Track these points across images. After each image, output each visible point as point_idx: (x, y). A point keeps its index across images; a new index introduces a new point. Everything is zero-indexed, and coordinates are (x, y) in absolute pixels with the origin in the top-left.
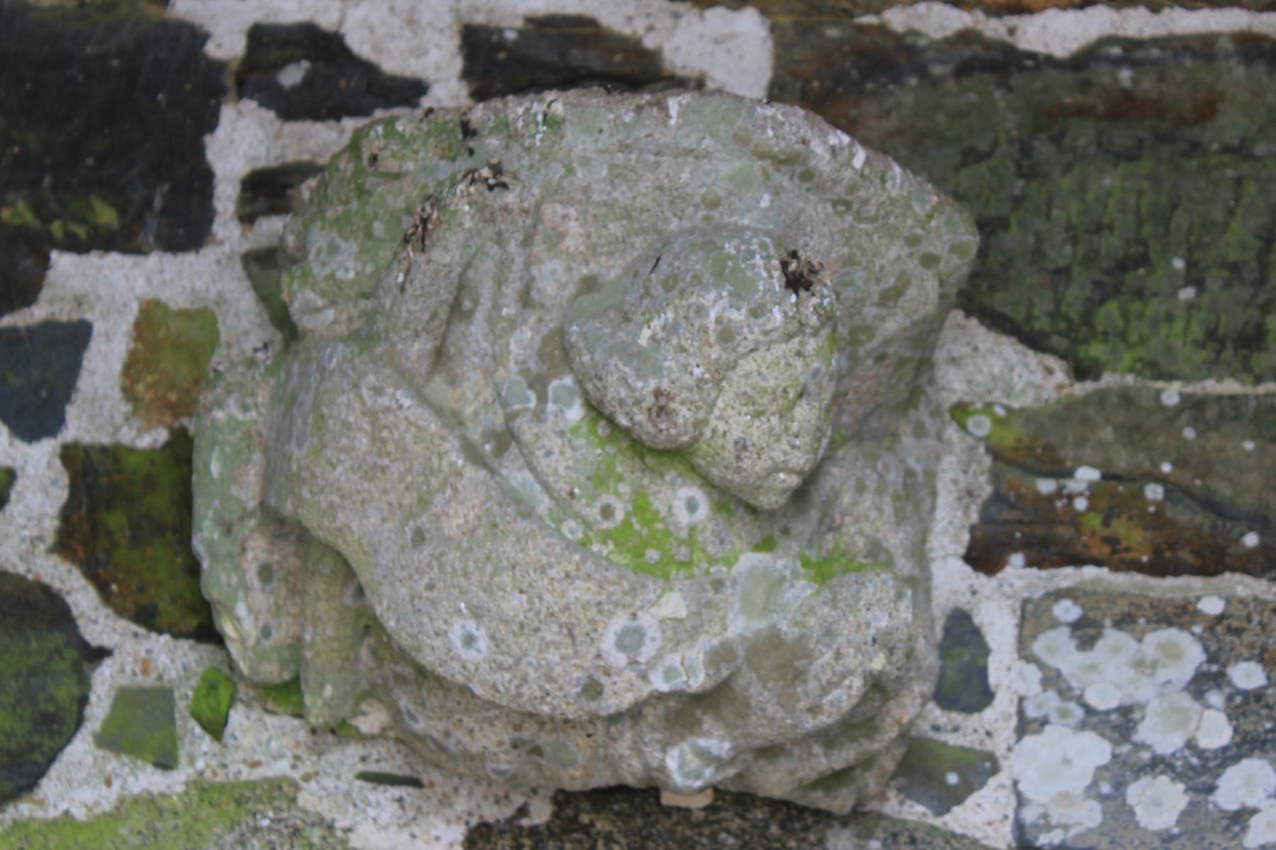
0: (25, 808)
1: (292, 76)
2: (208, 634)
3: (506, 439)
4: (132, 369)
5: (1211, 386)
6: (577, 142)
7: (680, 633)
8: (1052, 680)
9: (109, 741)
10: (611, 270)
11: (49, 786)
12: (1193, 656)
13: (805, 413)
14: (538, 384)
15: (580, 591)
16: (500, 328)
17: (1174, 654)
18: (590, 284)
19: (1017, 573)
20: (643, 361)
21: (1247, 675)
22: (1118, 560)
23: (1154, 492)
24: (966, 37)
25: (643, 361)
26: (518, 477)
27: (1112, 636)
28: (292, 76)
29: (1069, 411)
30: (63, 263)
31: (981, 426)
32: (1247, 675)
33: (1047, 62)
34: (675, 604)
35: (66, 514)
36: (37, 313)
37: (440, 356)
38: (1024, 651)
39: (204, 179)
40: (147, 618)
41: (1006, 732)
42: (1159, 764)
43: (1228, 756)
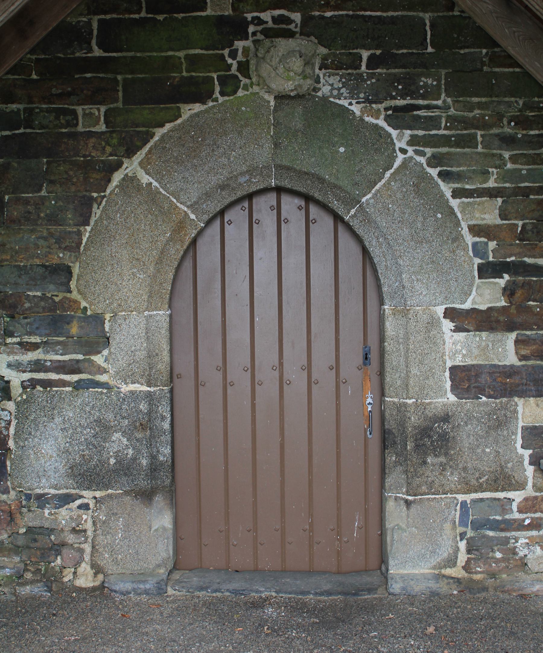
0: (236, 95)
1: (256, 22)
2: (250, 79)
3: (276, 68)
4: (243, 52)
5: (342, 51)
6: (282, 43)
7: (291, 85)
8: (326, 81)
9: (243, 89)
10: (285, 53)
11: (238, 93)
12: (339, 78)
13: (302, 67)
14: (279, 63)
15: (283, 82)
16: (276, 58)
17: (337, 78)
18: (283, 55)
19: (323, 71)
20: (288, 63)
21: (344, 80)
22: (332, 69)
23: (336, 62)
24: (320, 15)
25: (288, 63)
26: (278, 72)
27: (332, 77)
28: (256, 22)
29: (328, 55)
30: (236, 42)
31: (320, 56)
32: (344, 80)
33: (327, 17)
34: (291, 82)
35: (238, 67)
36: (234, 48)
37: (271, 61)
38: (324, 78)
39: (248, 33)
40: (245, 77)
41: (322, 86)
42: (336, 89)
43: (342, 88)
